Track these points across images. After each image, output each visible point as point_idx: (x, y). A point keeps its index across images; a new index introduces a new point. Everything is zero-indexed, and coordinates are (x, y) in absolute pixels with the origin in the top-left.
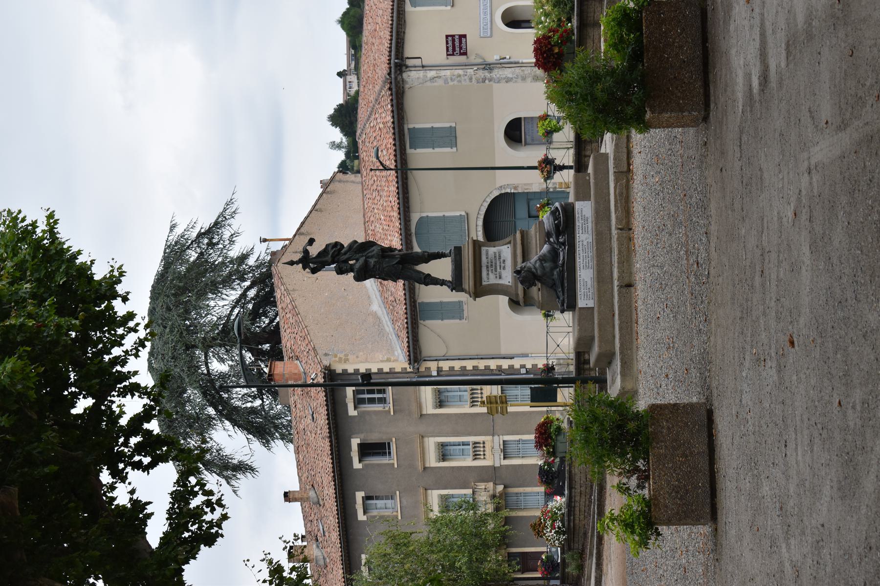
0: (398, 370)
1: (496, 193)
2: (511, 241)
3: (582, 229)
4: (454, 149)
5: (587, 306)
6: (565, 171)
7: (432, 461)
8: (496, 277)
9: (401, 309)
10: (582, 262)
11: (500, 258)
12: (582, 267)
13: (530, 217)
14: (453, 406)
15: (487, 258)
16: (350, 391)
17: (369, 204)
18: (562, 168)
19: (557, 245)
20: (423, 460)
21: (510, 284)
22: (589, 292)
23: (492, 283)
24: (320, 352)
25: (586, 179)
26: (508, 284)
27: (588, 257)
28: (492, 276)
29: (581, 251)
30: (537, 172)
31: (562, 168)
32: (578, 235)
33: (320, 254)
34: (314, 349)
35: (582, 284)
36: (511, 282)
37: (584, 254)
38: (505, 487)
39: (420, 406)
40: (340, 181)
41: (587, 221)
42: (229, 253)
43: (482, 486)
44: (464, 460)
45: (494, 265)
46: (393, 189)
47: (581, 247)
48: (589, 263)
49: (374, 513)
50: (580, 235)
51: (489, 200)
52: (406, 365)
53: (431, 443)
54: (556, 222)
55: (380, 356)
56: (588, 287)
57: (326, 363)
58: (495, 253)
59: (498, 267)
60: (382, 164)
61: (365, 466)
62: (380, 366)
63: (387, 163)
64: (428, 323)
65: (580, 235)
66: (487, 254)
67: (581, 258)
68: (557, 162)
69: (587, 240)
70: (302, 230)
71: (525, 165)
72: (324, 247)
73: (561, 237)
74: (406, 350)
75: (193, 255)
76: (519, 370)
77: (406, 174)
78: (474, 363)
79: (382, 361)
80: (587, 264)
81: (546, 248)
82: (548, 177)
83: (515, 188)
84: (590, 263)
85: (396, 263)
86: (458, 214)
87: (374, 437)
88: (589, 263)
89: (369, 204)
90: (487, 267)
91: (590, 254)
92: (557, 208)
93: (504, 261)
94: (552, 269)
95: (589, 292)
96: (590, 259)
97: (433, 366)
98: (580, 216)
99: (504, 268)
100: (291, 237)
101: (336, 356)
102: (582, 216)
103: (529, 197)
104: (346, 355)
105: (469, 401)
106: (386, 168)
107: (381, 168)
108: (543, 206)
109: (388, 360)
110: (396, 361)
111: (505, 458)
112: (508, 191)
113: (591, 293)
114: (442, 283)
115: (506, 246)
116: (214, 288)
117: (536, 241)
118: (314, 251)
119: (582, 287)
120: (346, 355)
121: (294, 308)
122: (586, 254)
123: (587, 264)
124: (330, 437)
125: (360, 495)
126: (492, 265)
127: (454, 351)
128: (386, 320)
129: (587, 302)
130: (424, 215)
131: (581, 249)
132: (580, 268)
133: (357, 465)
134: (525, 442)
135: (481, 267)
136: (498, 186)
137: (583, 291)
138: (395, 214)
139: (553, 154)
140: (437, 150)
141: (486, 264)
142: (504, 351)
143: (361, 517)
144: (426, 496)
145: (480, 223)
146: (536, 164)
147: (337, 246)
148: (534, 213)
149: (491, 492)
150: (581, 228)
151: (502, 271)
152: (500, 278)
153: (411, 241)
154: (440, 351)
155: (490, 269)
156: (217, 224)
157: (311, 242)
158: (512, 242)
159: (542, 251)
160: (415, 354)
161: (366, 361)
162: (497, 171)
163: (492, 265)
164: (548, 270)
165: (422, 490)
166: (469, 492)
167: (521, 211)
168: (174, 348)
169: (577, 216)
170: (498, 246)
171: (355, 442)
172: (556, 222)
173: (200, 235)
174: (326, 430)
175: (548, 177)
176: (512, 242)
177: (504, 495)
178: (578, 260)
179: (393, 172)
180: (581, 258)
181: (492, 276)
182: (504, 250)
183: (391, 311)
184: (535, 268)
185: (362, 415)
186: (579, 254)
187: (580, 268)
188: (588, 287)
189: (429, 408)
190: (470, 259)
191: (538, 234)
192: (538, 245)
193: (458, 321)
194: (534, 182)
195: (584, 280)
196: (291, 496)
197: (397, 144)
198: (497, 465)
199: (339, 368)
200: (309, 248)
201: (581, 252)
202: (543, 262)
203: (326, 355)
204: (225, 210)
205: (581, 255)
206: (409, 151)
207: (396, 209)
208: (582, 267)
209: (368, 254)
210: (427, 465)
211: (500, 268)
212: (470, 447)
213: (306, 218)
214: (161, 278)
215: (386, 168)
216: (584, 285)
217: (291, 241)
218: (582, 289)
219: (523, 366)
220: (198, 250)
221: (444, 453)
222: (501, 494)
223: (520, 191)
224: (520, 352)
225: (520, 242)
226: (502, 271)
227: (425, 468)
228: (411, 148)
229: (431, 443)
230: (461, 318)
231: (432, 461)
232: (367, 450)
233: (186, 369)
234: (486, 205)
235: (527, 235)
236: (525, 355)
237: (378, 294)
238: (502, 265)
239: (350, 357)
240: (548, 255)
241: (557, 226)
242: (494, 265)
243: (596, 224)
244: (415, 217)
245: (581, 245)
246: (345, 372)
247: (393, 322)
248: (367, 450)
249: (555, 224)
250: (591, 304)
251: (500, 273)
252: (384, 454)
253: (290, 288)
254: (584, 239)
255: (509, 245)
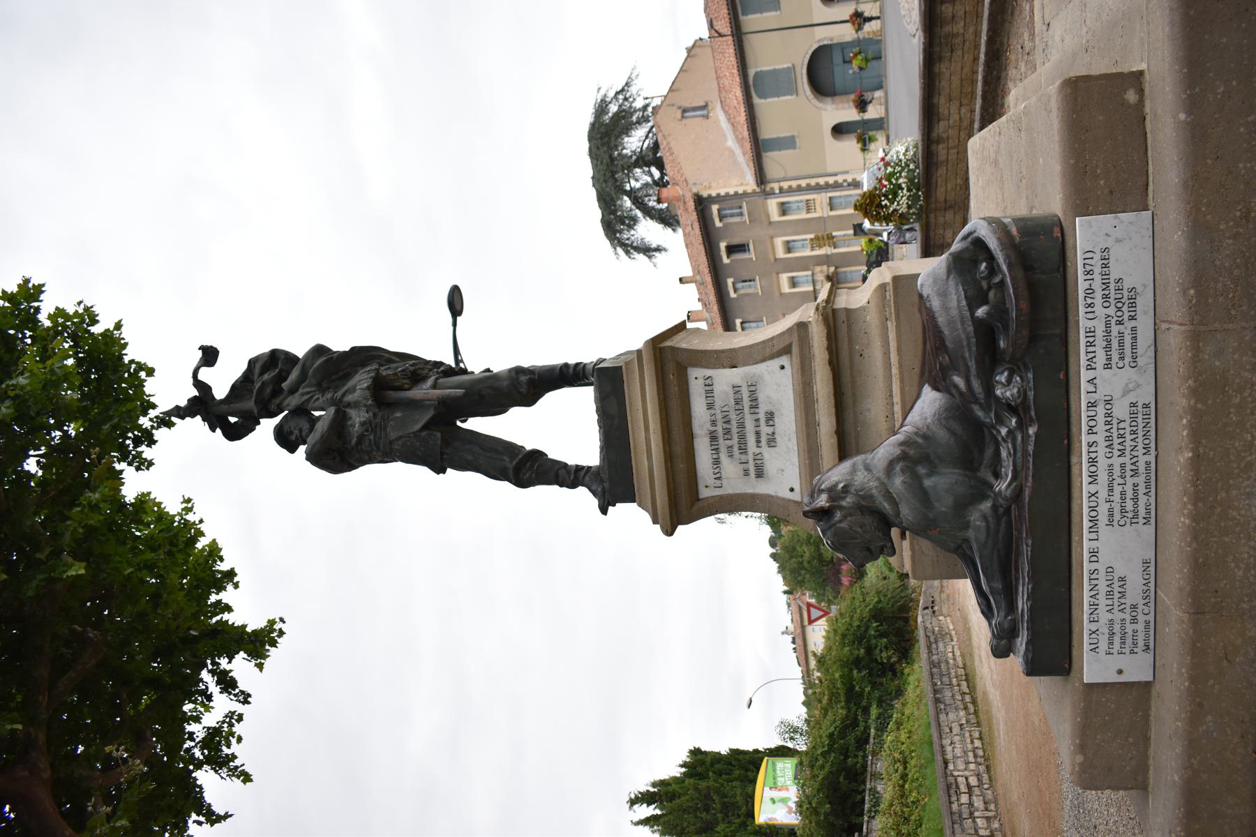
0: (750, 191)
1: (815, 46)
2: (790, 346)
3: (1108, 348)
4: (779, 12)
5: (1122, 679)
6: (874, 22)
7: (781, 253)
8: (746, 472)
9: (748, 145)
10: (1103, 494)
11: (754, 406)
12: (1103, 519)
13: (845, 62)
14: (794, 214)
15: (710, 406)
16: (715, 208)
17: (718, 63)
18: (870, 19)
19: (986, 408)
20: (774, 253)
21: (796, 496)
22: (1134, 620)
23: (730, 491)
24: (690, 182)
25: (1124, 104)
26: (789, 495)
27: (1135, 473)
28: (730, 468)
29: (1102, 444)
30: (849, 25)
31: (870, 19)
32: (1085, 375)
33: (238, 389)
34: (686, 180)
35: (1103, 588)
36: (797, 487)
37: (1117, 461)
38: (836, 268)
39: (768, 216)
40: (699, 46)
41: (1133, 305)
42: (633, 105)
43: (818, 269)
44: (804, 251)
45: (734, 430)
46: (732, 50)
47: (1101, 428)
48: (1135, 499)
49: (742, 292)
50: (1100, 372)
51: (810, 52)
52: (755, 187)
53: (779, 242)
54: (981, 312)
55: (735, 182)
56: (1129, 601)
57: (695, 190)
58: (736, 389)
59: (751, 439)
60: (717, 31)
61: (731, 261)
62: (736, 189)
63: (722, 31)
64: (770, 154)
65: (1100, 372)
66: (709, 393)
67: (1103, 477)
68: (867, 14)
69: (1132, 398)
70: (673, 87)
71: (838, 20)
72: (244, 367)
73: (1002, 378)
74: (754, 176)
75: (613, 108)
76: (842, 184)
77: (741, 37)
78: (807, 181)
79: (737, 186)
80: (1129, 505)
81: (929, 402)
82: (859, 28)
83: (831, 40)
84: (1142, 500)
85: (425, 427)
86: (785, 66)
87: (736, 241)
88: (1135, 499)
89: (718, 63)
90: (713, 438)
91: (1142, 460)
92: (979, 244)
93: (770, 416)
94: (962, 506)
95: (1134, 620)
96: (1141, 480)
97: (776, 186)
98: (1097, 285)
99: (772, 442)
100: (665, 94)
101: (702, 184)
102: (1106, 285)
103: (843, 46)
104: (710, 183)
105: (805, 209)
106: (721, 35)
107: (716, 35)
108: (856, 55)
109: (741, 184)
110: (747, 184)
111: (831, 210)
112: (826, 43)
113: (1140, 627)
114: (567, 476)
115: (774, 364)
116: (627, 130)
117: (887, 353)
118: (221, 381)
119: (1102, 601)
120: (710, 183)
121: (670, 149)
122: (1126, 459)
123: (1129, 505)
124: (704, 243)
125: (730, 281)
126: (727, 432)
127: (791, 174)
128: (738, 152)
129: (1124, 661)
130: (759, 69)
131: (1100, 438)
132: (1093, 520)
133: (726, 260)
134: (848, 235)
135: (690, 437)
136: (817, 39)
137: (1104, 617)
138: (735, 71)
139: (862, 8)
140: (765, 14)
141: (708, 426)
142: (830, 170)
143: (733, 295)
144: (778, 278)
145: (805, 71)
146: (848, 18)
147: (276, 361)
148: (847, 59)
149: (826, 273)
150: (1100, 342)
151: (766, 451)
152: (760, 474)
153: (750, 92)
154: (781, 175)
155: (723, 444)
156: (627, 84)
157: (210, 356)
158: (795, 349)
159: (915, 416)
160: (761, 178)
161: (725, 187)
162: (816, 28)
163: (727, 432)
164: (943, 504)
165: (774, 275)
166: (809, 273)
167: (837, 58)
168: (605, 174)
169: (1082, 286)
170: (744, 365)
171: (723, 245)
172: (981, 312)
173: (617, 93)
174: (700, 240)
175: (859, 28)
176: (795, 349)
177: (836, 273)
178: (1084, 487)
179: (730, 38)
180: (1103, 477)
181: (730, 468)
182: (767, 377)
183: (742, 146)
184: (888, 496)
185: (726, 226)
186: (1093, 462)
187: (1093, 520)
188: (1129, 601)
189: (775, 216)
190: (652, 437)
191: (891, 326)
192: (895, 371)
193: (791, 151)
194: (846, 33)
195: (1110, 570)
196: (684, 280)
197: (731, 13)
198: (826, 215)
199: (705, 194)
200: (205, 375)
201: (1102, 449)
202: (922, 470)
203: (695, 184)
204: (631, 74)
205: (1103, 463)
206: (742, 18)
207: (735, 67)
208: (1103, 519)
209: (344, 395)
210: (777, 257)
211: (758, 441)
212: (808, 242)
213: (676, 78)
214: (593, 126)
215: (721, 35)
216: (1109, 594)
217: (665, 97)
218: (1102, 609)
219: (845, 181)
220: (617, 104)
221: (789, 247)
222: (833, 273)
223: (835, 42)
224: (842, 170)
225: (826, 356)
226: (767, 453)
227: (776, 259)
228: (743, 14)
229: (779, 242)
230: (794, 148)
231: (781, 253)
232: (731, 250)
233: (613, 188)
234: (808, 57)
235: (849, 327)
236: (846, 172)
237: (732, 132)
238: (765, 430)
239: (713, 184)
240: (942, 435)
241: (986, 333)
242: (734, 430)
243: (1196, 339)
244: (751, 72)
245: (1101, 418)
246: (710, 196)
247: (744, 154)
248: (731, 250)
249: (978, 323)
250: (1137, 669)
251: (758, 459)
252: (745, 251)
253: (666, 134)
254: (1117, 394)
255: (784, 360)
